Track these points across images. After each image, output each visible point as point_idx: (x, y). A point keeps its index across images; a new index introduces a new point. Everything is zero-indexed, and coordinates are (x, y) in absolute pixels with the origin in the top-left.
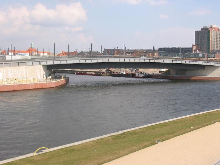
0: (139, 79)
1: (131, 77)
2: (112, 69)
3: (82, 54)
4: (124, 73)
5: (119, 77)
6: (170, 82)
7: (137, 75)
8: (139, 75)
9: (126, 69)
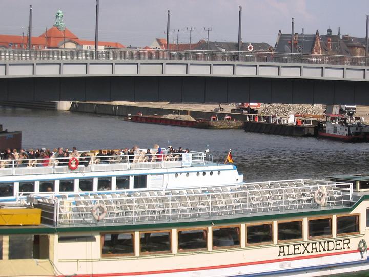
0: (338, 147)
1: (309, 136)
2: (256, 104)
3: (204, 50)
4: (291, 120)
5: (269, 133)
6: (238, 129)
7: (329, 128)
8: (335, 128)
9: (272, 104)
